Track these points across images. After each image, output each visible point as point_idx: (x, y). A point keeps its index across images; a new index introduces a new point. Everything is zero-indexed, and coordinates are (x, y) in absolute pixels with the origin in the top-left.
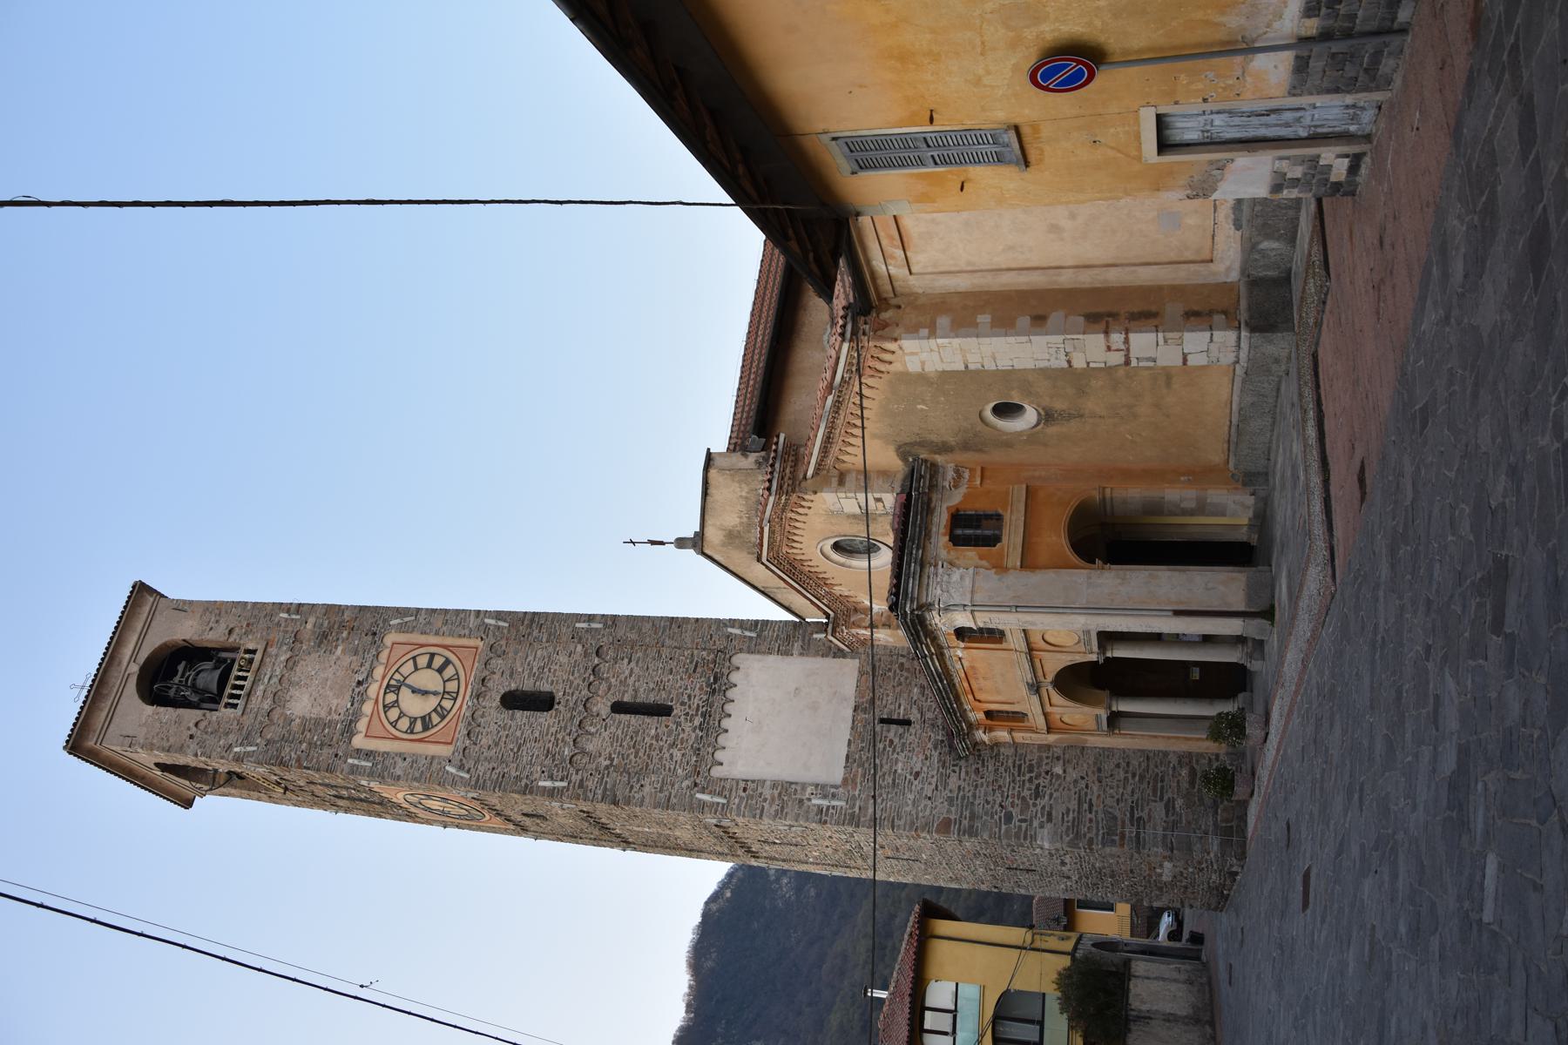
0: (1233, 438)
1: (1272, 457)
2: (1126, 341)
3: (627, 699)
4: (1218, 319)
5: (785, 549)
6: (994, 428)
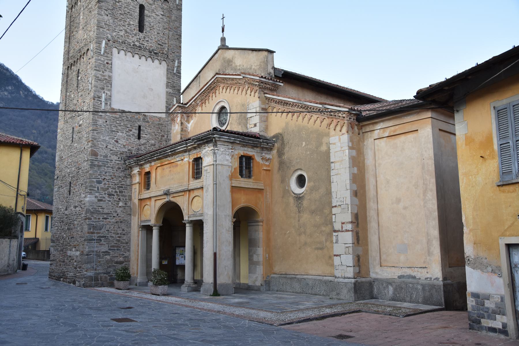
0: (288, 276)
1: (278, 292)
2: (347, 231)
3: (146, 12)
4: (357, 268)
5: (222, 85)
6: (292, 175)
